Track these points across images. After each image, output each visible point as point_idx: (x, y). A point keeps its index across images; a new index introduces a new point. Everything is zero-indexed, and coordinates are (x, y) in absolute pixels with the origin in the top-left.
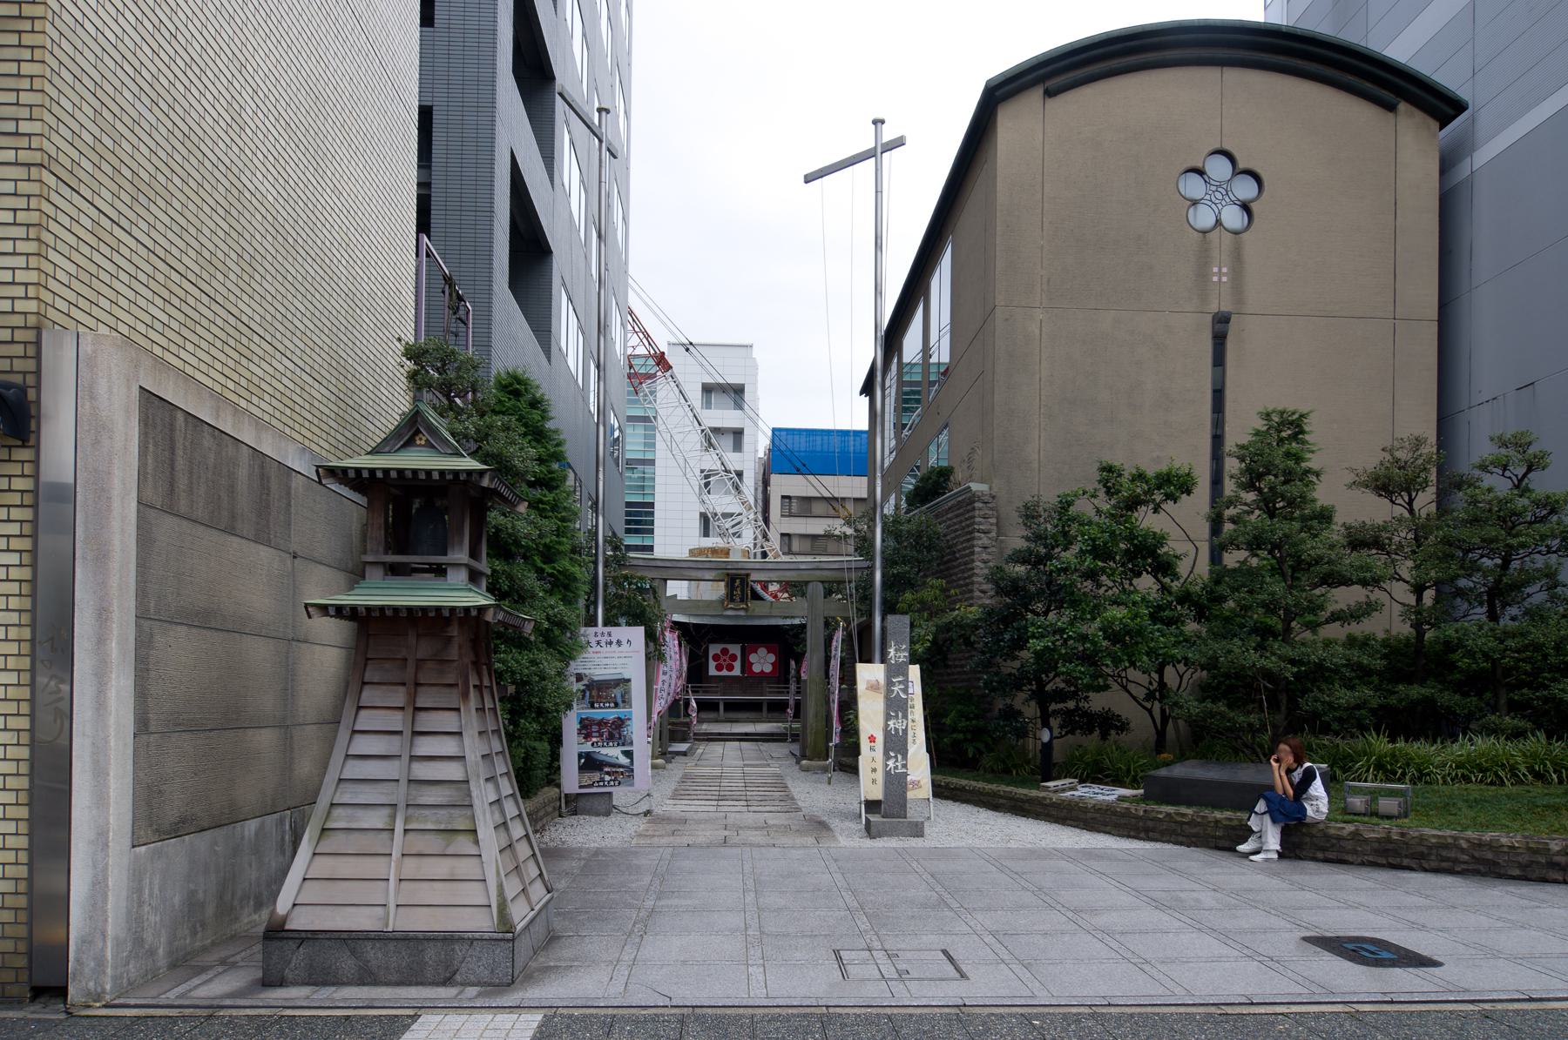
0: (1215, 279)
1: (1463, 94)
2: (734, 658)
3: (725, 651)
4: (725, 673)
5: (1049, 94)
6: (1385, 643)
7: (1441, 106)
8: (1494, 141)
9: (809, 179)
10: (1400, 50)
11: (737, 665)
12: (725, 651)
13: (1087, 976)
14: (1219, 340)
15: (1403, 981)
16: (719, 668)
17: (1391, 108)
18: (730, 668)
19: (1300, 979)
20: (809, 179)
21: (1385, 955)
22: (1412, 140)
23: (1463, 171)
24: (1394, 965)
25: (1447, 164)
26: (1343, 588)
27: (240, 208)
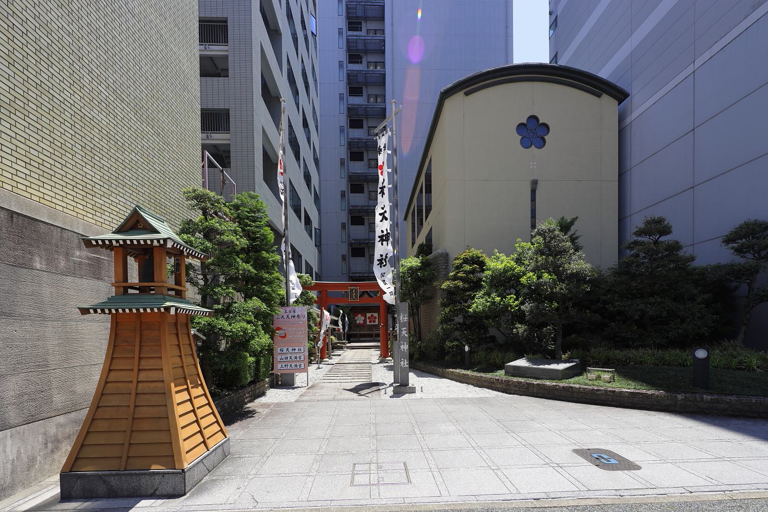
0: (531, 167)
1: (627, 90)
2: (375, 318)
3: (372, 316)
4: (372, 323)
5: (467, 94)
6: (675, 247)
7: (620, 95)
8: (639, 106)
9: (535, 183)
10: (604, 74)
11: (377, 320)
12: (372, 316)
13: (475, 483)
14: (533, 192)
15: (621, 479)
16: (370, 322)
17: (599, 96)
18: (374, 322)
19: (572, 480)
20: (535, 183)
21: (613, 461)
22: (608, 104)
23: (628, 121)
24: (618, 469)
25: (621, 118)
26: (454, 382)
27: (189, 147)
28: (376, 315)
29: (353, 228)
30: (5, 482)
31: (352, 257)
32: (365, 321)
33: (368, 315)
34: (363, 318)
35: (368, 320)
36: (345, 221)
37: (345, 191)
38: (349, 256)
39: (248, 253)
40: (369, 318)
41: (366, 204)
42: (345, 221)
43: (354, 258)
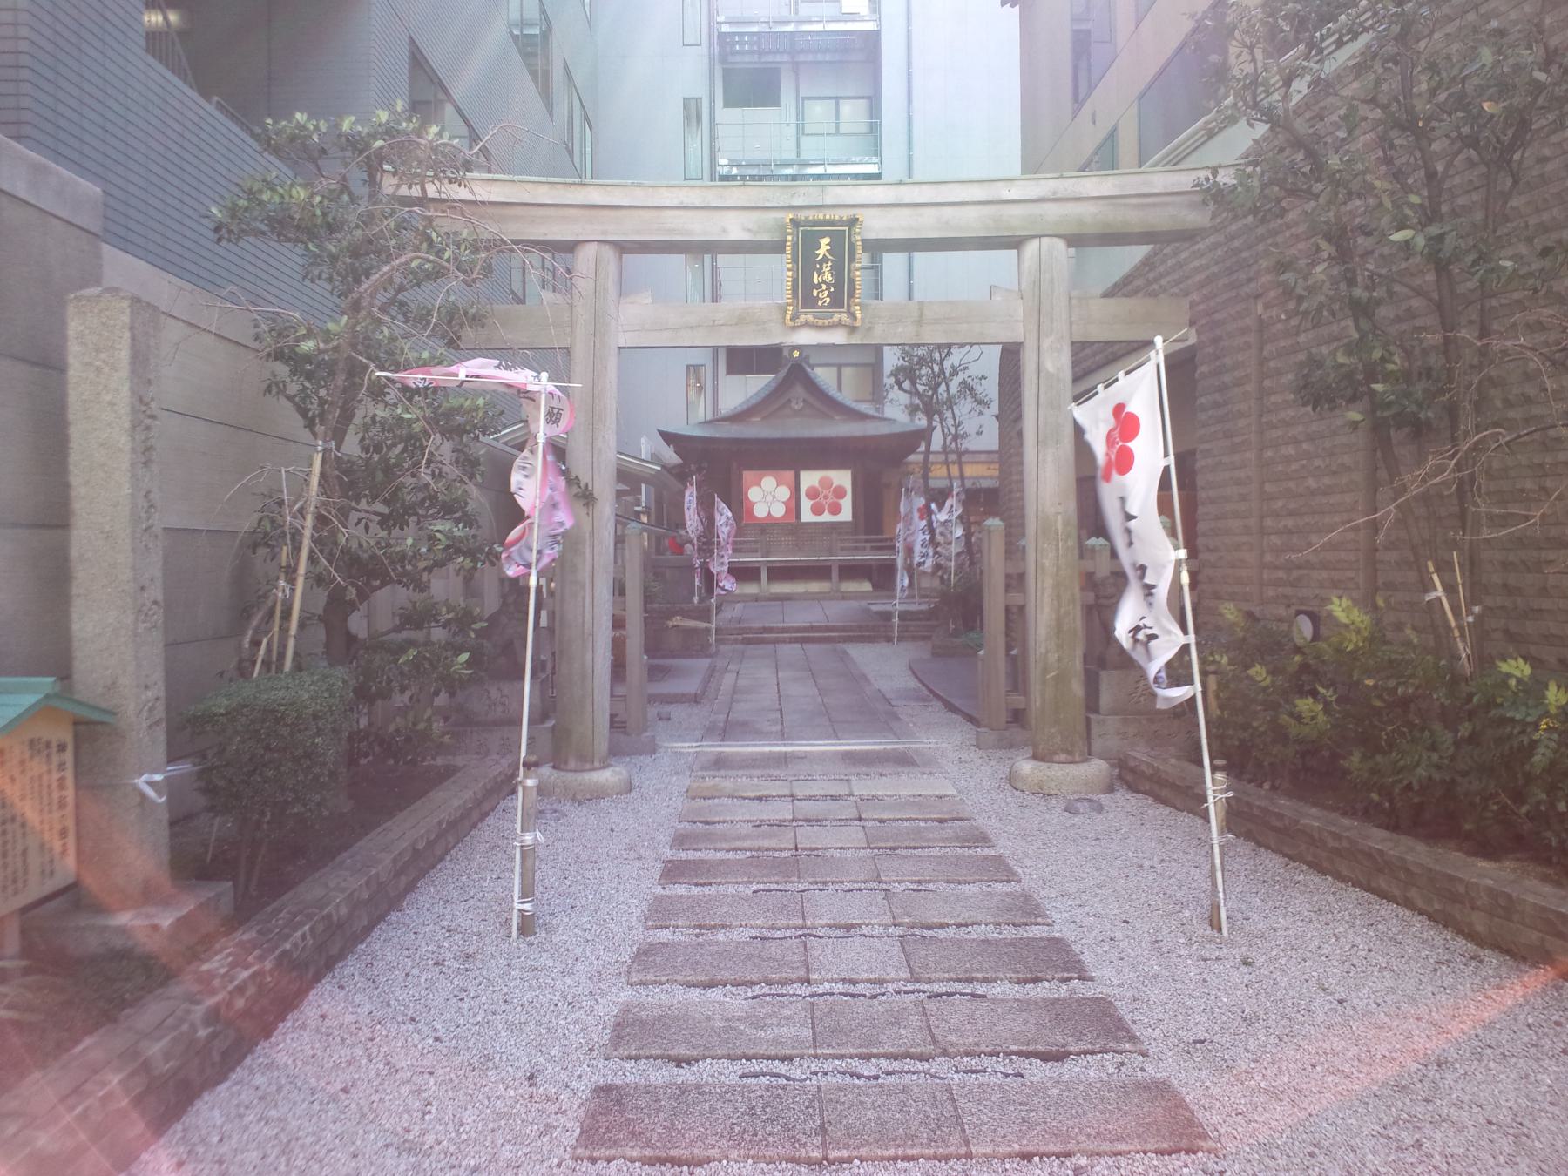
3: (826, 483)
4: (826, 517)
16: (817, 510)
18: (836, 509)
28: (846, 515)
29: (730, 119)
30: (455, 166)
31: (727, 105)
32: (794, 506)
33: (810, 479)
34: (784, 493)
35: (806, 504)
36: (701, 91)
37: (698, 100)
38: (712, 100)
39: (825, 1158)
40: (813, 494)
41: (790, 155)
42: (701, 91)
43: (736, 112)
